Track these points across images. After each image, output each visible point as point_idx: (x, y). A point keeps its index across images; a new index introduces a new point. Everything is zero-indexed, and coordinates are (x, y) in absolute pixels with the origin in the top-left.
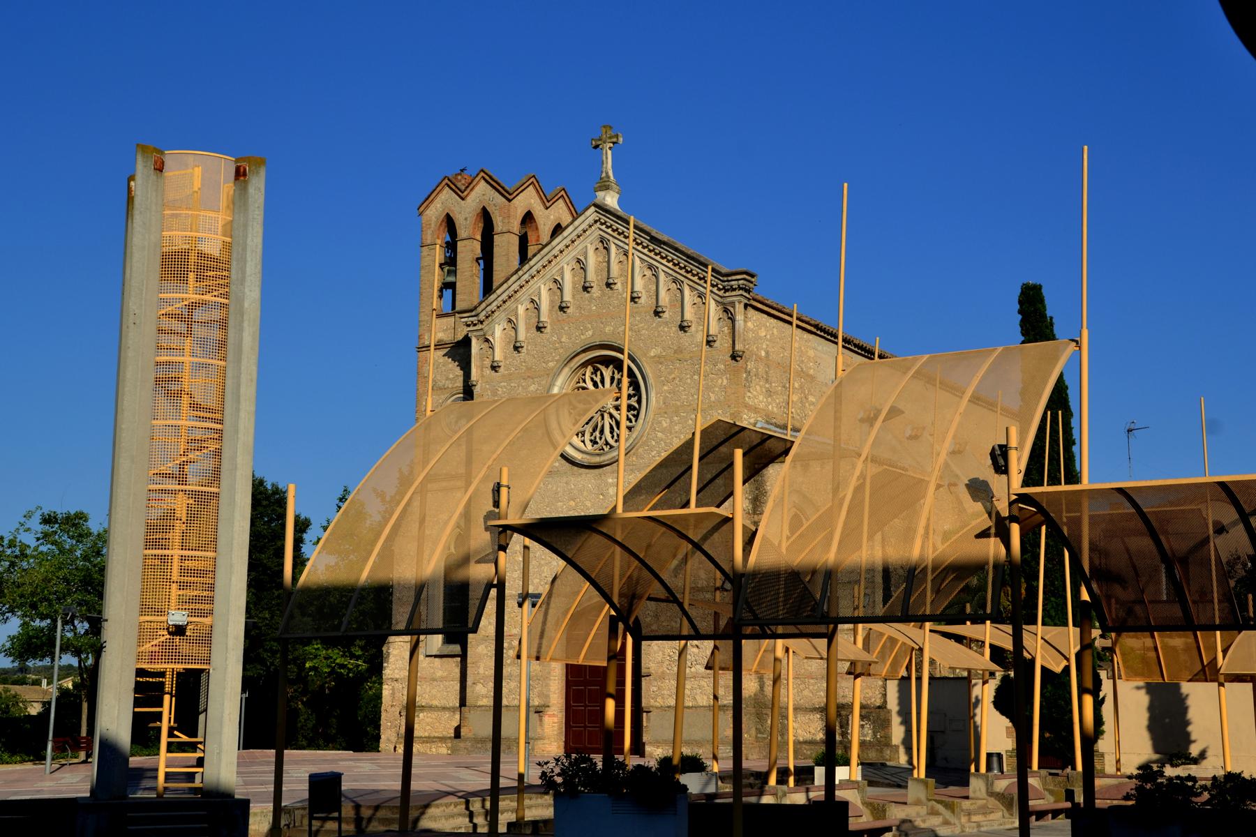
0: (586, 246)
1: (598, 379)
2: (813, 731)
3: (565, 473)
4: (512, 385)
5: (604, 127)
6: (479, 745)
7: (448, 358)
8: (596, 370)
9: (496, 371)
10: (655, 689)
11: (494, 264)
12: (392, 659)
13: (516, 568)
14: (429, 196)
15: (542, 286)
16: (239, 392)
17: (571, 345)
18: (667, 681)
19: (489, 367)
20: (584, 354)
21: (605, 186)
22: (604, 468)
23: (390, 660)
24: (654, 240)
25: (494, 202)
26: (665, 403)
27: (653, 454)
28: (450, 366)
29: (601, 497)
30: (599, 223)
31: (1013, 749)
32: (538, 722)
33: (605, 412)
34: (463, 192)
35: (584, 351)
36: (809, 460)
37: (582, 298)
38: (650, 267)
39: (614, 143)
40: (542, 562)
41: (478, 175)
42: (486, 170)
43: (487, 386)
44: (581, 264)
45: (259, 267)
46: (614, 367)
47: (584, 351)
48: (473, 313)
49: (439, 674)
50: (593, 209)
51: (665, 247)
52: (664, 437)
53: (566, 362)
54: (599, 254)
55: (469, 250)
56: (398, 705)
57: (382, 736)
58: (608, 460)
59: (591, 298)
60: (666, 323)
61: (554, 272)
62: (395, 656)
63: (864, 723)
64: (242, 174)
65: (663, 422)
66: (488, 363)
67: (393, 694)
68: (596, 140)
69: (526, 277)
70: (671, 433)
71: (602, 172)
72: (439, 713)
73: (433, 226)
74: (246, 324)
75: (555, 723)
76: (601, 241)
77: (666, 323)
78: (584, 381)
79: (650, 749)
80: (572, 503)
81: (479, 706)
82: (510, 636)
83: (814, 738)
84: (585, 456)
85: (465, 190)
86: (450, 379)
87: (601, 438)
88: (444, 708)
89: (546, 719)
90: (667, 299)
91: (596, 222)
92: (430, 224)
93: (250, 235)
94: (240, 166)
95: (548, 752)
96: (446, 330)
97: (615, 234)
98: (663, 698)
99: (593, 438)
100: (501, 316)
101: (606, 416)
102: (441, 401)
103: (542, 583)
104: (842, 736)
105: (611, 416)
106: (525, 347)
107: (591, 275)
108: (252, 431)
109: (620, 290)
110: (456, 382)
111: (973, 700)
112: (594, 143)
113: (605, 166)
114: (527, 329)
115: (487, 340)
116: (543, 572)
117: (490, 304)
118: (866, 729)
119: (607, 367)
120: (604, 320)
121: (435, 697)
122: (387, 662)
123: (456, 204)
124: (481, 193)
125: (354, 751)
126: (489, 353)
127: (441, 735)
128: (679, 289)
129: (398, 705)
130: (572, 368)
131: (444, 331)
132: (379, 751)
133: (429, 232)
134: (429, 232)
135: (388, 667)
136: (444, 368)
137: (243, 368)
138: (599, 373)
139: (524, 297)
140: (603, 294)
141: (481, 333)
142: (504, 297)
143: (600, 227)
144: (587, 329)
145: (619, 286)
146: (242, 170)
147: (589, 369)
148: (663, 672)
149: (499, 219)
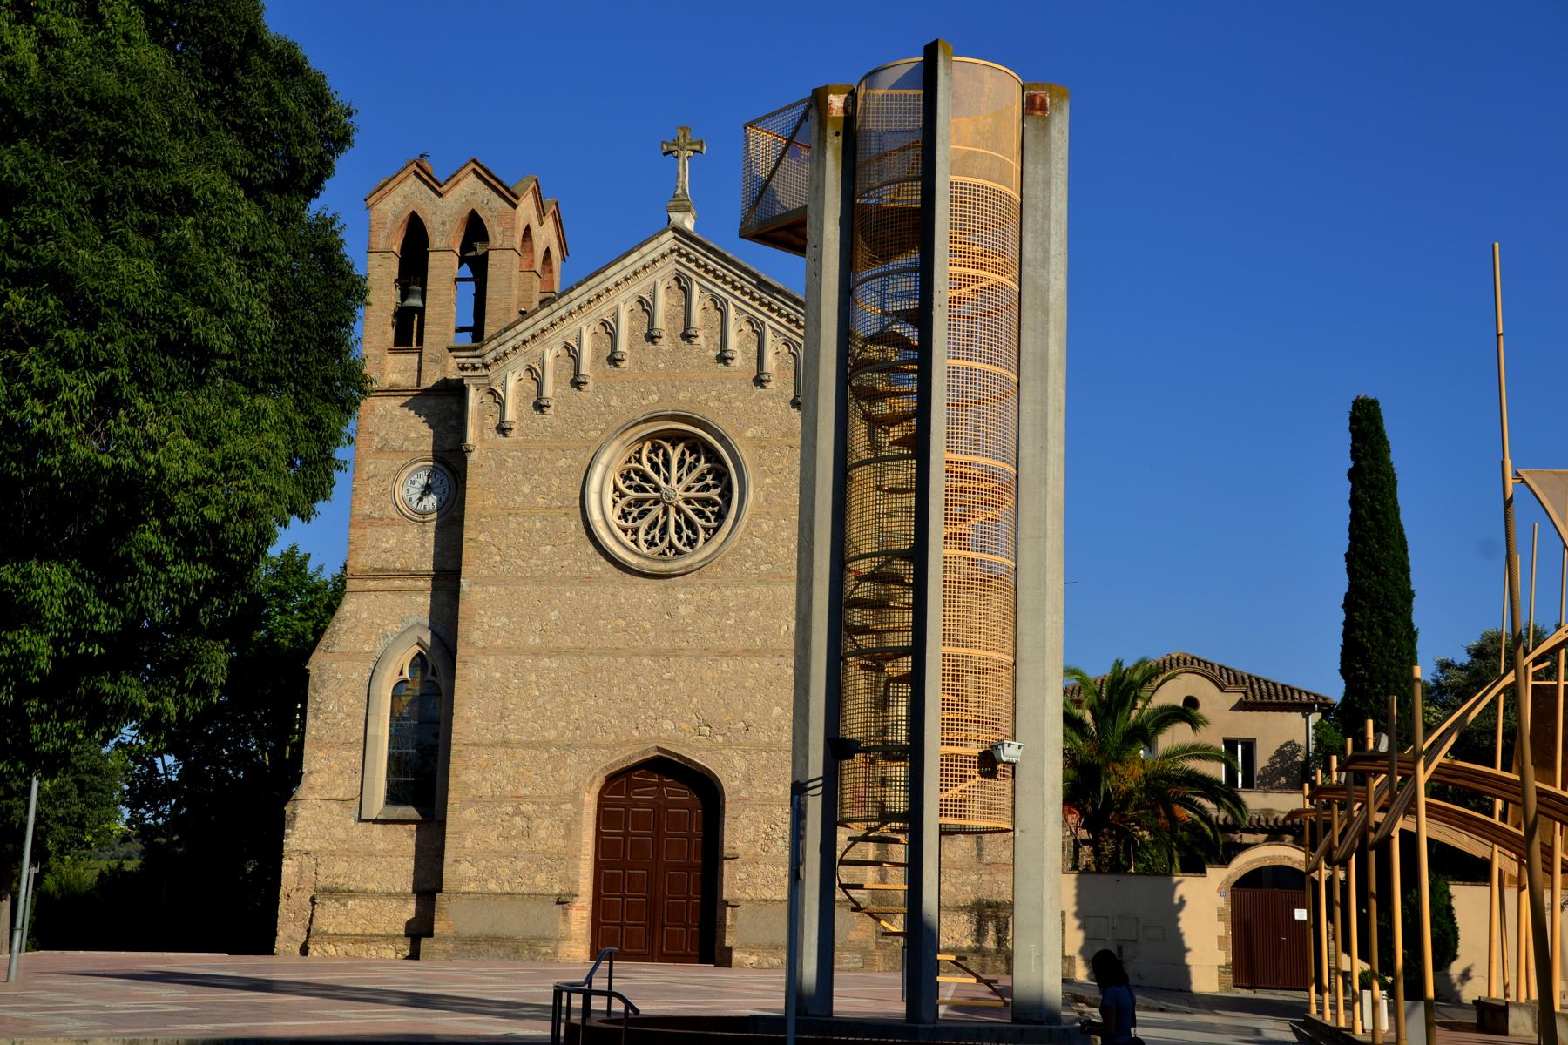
0: (655, 283)
1: (660, 460)
2: (957, 937)
4: (530, 456)
5: (682, 128)
6: (468, 947)
7: (410, 409)
8: (655, 449)
9: (505, 435)
10: (743, 876)
11: (488, 289)
12: (299, 823)
13: (530, 705)
14: (385, 185)
15: (585, 328)
16: (1046, 424)
17: (624, 411)
18: (762, 866)
19: (494, 429)
20: (644, 425)
21: (684, 206)
22: (673, 579)
23: (297, 825)
24: (762, 284)
26: (767, 500)
27: (748, 565)
28: (412, 421)
29: (667, 617)
30: (675, 254)
31: (1227, 965)
32: (561, 917)
33: (664, 502)
34: (440, 186)
35: (645, 421)
38: (751, 321)
39: (695, 151)
40: (572, 699)
41: (466, 165)
42: (478, 161)
43: (490, 455)
44: (646, 306)
45: (1065, 245)
46: (686, 447)
47: (645, 421)
48: (477, 353)
49: (381, 846)
50: (670, 234)
51: (779, 297)
54: (671, 294)
55: (443, 266)
56: (308, 888)
57: (280, 933)
58: (681, 569)
60: (772, 397)
61: (603, 310)
64: (1038, 107)
65: (764, 525)
66: (492, 422)
67: (301, 872)
68: (667, 144)
69: (562, 312)
70: (775, 540)
71: (677, 187)
72: (381, 901)
73: (388, 225)
74: (1051, 326)
75: (583, 918)
76: (676, 279)
77: (772, 397)
78: (639, 461)
80: (621, 623)
81: (463, 893)
83: (959, 945)
84: (642, 561)
85: (445, 184)
86: (412, 440)
87: (661, 540)
88: (389, 895)
90: (774, 365)
91: (672, 251)
92: (385, 223)
93: (1053, 197)
94: (1035, 95)
95: (575, 957)
96: (406, 370)
97: (701, 271)
98: (755, 888)
99: (649, 537)
101: (672, 510)
102: (395, 468)
104: (999, 944)
105: (679, 511)
106: (553, 407)
107: (660, 322)
108: (1062, 484)
109: (704, 345)
110: (420, 444)
111: (1176, 901)
112: (665, 147)
113: (681, 179)
114: (556, 384)
115: (492, 392)
116: (573, 713)
117: (503, 344)
119: (674, 446)
120: (677, 383)
121: (366, 879)
122: (293, 828)
123: (428, 201)
124: (467, 192)
125: (230, 953)
126: (494, 409)
127: (384, 933)
128: (793, 354)
129: (308, 888)
130: (625, 442)
131: (400, 372)
132: (274, 954)
133: (383, 234)
134: (383, 234)
135: (293, 834)
136: (401, 424)
137: (1050, 389)
138: (661, 452)
139: (556, 340)
140: (677, 348)
141: (485, 381)
142: (526, 335)
143: (678, 258)
144: (650, 393)
145: (701, 340)
146: (1038, 101)
147: (648, 445)
148: (756, 854)
149: (498, 230)
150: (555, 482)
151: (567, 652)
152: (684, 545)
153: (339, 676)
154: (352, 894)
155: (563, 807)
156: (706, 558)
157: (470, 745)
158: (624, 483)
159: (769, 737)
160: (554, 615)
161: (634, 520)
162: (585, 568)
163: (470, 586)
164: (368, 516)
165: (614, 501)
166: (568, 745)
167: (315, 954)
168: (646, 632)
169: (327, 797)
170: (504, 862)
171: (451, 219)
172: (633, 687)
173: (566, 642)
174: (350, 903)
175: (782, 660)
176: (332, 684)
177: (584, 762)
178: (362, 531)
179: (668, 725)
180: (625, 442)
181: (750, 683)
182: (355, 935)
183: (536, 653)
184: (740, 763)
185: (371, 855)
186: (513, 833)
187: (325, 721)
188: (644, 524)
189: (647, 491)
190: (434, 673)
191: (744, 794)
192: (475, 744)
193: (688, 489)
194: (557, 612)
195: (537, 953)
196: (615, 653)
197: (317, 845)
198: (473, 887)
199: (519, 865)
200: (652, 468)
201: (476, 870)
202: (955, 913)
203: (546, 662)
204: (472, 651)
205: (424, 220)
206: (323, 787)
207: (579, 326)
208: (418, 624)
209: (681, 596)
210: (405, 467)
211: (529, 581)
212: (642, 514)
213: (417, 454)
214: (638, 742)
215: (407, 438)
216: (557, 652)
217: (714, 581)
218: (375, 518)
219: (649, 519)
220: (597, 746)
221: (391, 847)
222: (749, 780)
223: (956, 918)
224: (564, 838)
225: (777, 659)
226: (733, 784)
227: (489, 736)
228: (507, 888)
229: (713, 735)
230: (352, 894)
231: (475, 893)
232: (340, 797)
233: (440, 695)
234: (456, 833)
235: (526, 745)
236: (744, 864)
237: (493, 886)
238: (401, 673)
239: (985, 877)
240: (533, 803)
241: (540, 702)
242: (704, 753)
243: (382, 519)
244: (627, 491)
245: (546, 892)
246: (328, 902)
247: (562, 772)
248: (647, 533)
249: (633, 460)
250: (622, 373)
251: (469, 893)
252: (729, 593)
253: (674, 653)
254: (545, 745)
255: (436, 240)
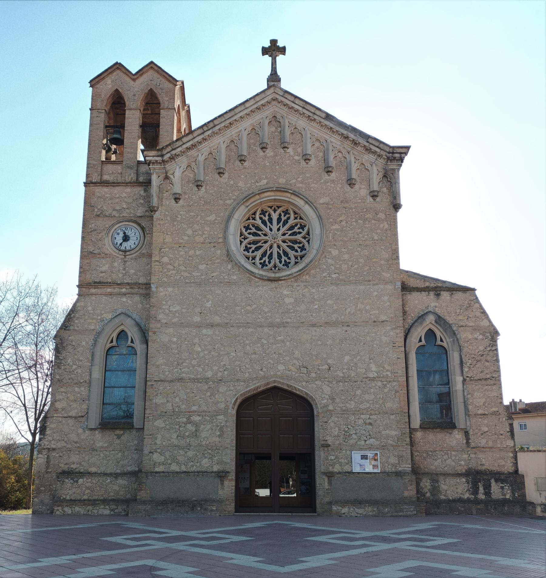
3: (243, 284)
10: (333, 458)
23: (47, 433)
25: (161, 86)
27: (324, 275)
36: (440, 291)
37: (256, 156)
43: (167, 213)
49: (99, 444)
52: (333, 263)
53: (245, 200)
59: (266, 156)
61: (233, 133)
62: (51, 429)
63: (503, 485)
75: (232, 486)
78: (254, 219)
79: (336, 509)
81: (156, 472)
82: (189, 412)
83: (462, 496)
88: (106, 474)
89: (226, 483)
100: (183, 161)
103: (221, 370)
118: (506, 490)
127: (102, 498)
130: (247, 206)
139: (205, 149)
144: (261, 179)
150: (207, 229)
151: (218, 325)
152: (283, 265)
153: (74, 343)
154: (81, 474)
155: (218, 417)
156: (300, 271)
157: (159, 381)
158: (246, 231)
159: (343, 373)
160: (208, 304)
161: (253, 252)
162: (226, 277)
163: (157, 288)
164: (91, 252)
165: (240, 241)
166: (220, 380)
167: (58, 513)
168: (266, 313)
169: (65, 415)
170: (182, 452)
171: (139, 93)
172: (259, 345)
173: (217, 319)
174: (81, 481)
175: (348, 328)
176: (70, 348)
177: (230, 390)
178: (88, 261)
179: (281, 367)
180: (247, 206)
181: (330, 342)
182: (84, 500)
183: (199, 326)
184: (327, 389)
185: (94, 450)
186: (187, 434)
187: (64, 369)
188: (259, 254)
189: (260, 236)
190: (132, 341)
191: (331, 408)
192: (161, 381)
193: (284, 234)
194: (210, 302)
195: (206, 509)
196: (247, 325)
197: (59, 445)
198: (161, 469)
199: (190, 454)
200: (262, 222)
201: (163, 458)
202: (458, 478)
203: (204, 331)
204: (159, 325)
205: (123, 94)
206: (63, 409)
207: (219, 141)
208: (122, 313)
209: (285, 292)
210: (113, 225)
211: (193, 285)
212: (257, 249)
213: (121, 218)
214: (264, 377)
215: (114, 210)
216: (212, 326)
217: (305, 284)
218: (95, 254)
219: (262, 251)
220: (238, 380)
221: (106, 445)
222: (333, 399)
223: (458, 481)
224: (219, 436)
225: (345, 328)
226: (323, 402)
227: (170, 376)
228: (184, 469)
229: (309, 372)
230: (81, 474)
231: (163, 472)
232: (74, 415)
233: (137, 354)
234: (150, 435)
235: (194, 380)
236: (333, 450)
237: (174, 468)
238: (112, 342)
239: (473, 456)
240: (199, 415)
241: (202, 354)
242: (304, 383)
243: (100, 254)
244: (248, 235)
245: (208, 470)
246: (67, 480)
247: (217, 396)
248: (261, 259)
249: (251, 218)
250: (245, 168)
251: (159, 472)
252: (314, 291)
253: (284, 325)
254: (207, 380)
255: (129, 103)
